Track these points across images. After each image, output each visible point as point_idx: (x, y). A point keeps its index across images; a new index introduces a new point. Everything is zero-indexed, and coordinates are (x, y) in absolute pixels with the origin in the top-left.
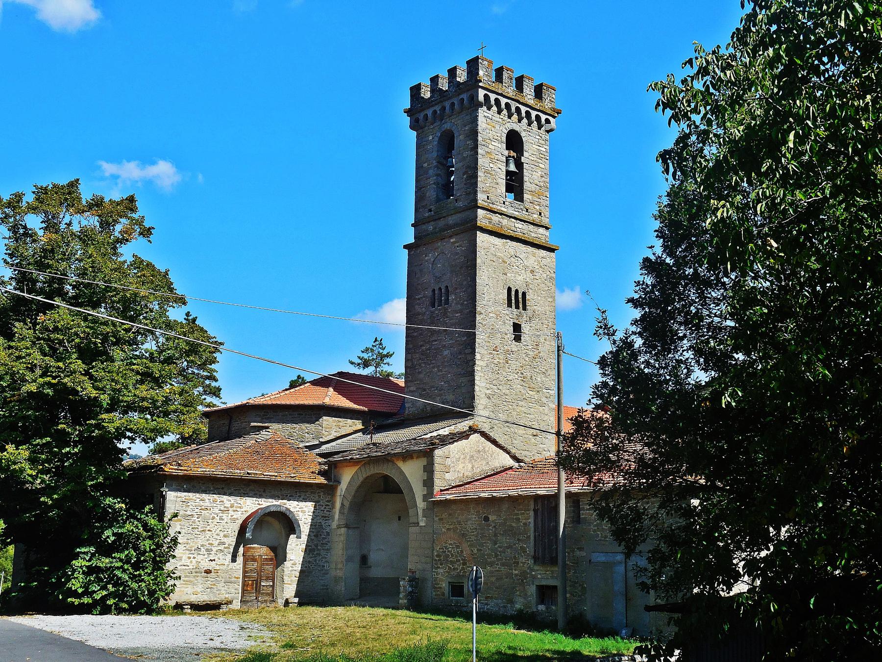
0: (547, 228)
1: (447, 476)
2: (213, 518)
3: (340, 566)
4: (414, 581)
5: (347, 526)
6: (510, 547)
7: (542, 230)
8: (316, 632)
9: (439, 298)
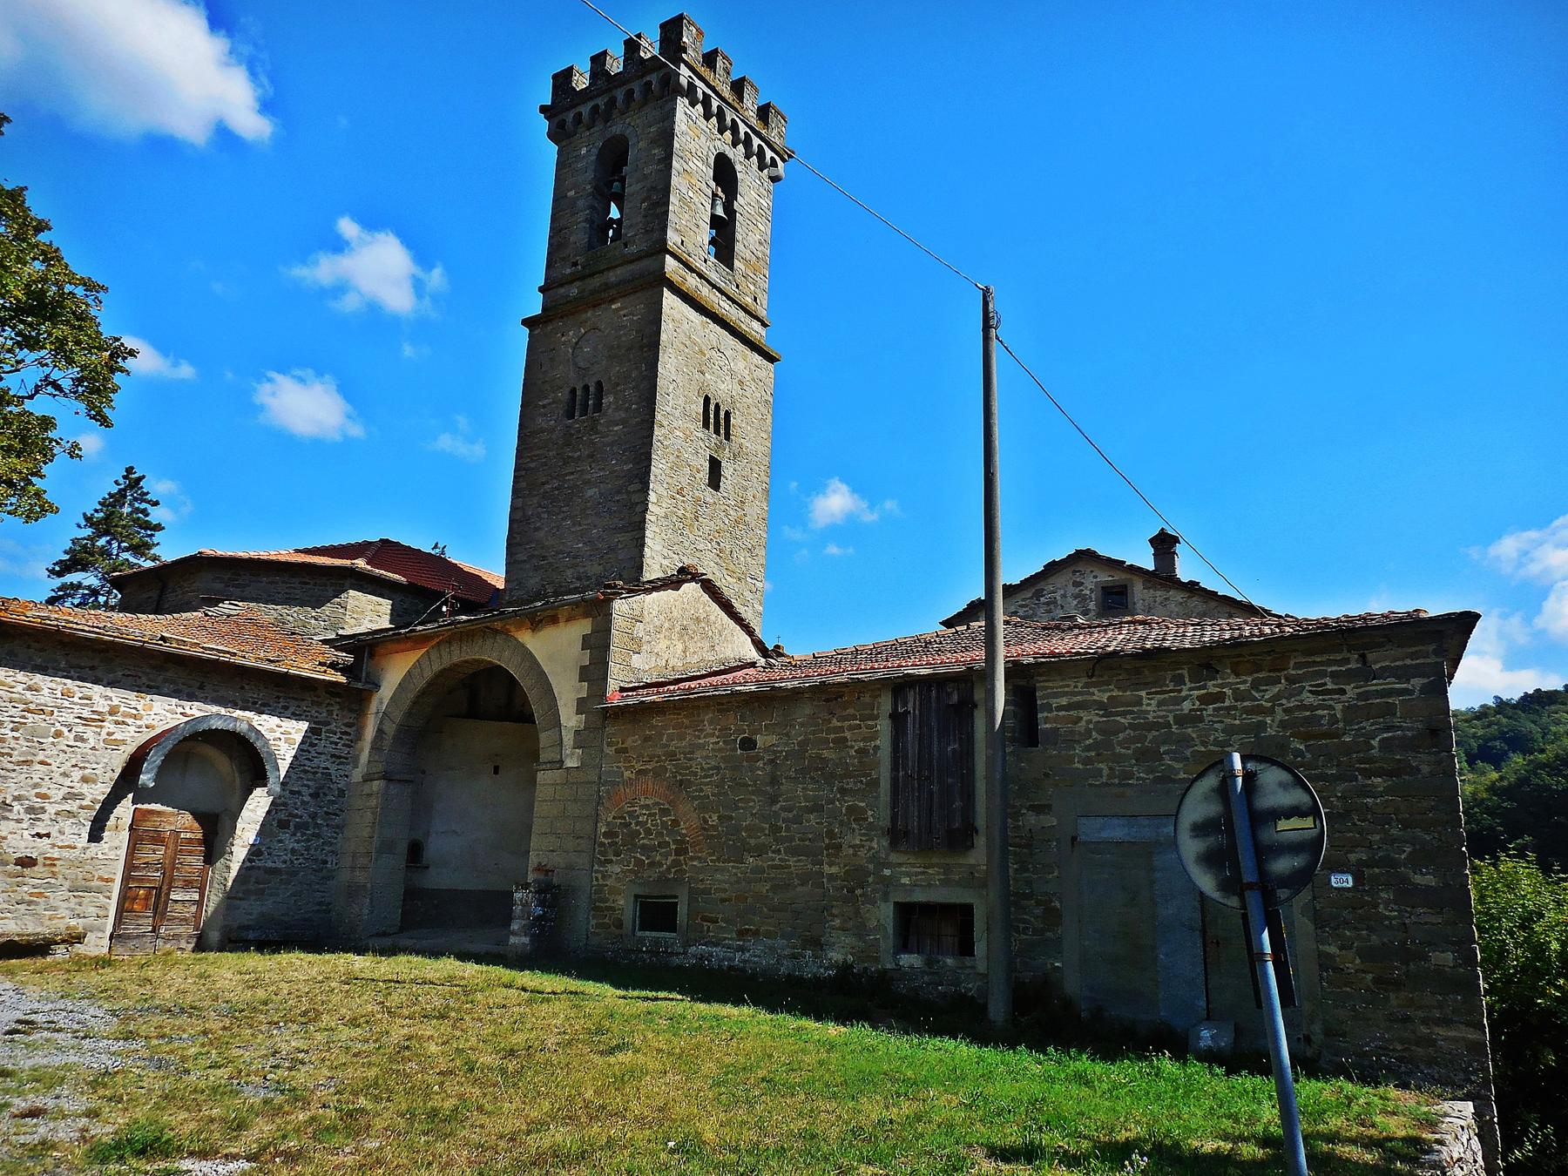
0: (764, 325)
1: (636, 660)
2: (58, 734)
3: (362, 861)
4: (552, 894)
5: (387, 777)
6: (816, 808)
7: (756, 325)
8: (289, 1040)
9: (584, 401)
